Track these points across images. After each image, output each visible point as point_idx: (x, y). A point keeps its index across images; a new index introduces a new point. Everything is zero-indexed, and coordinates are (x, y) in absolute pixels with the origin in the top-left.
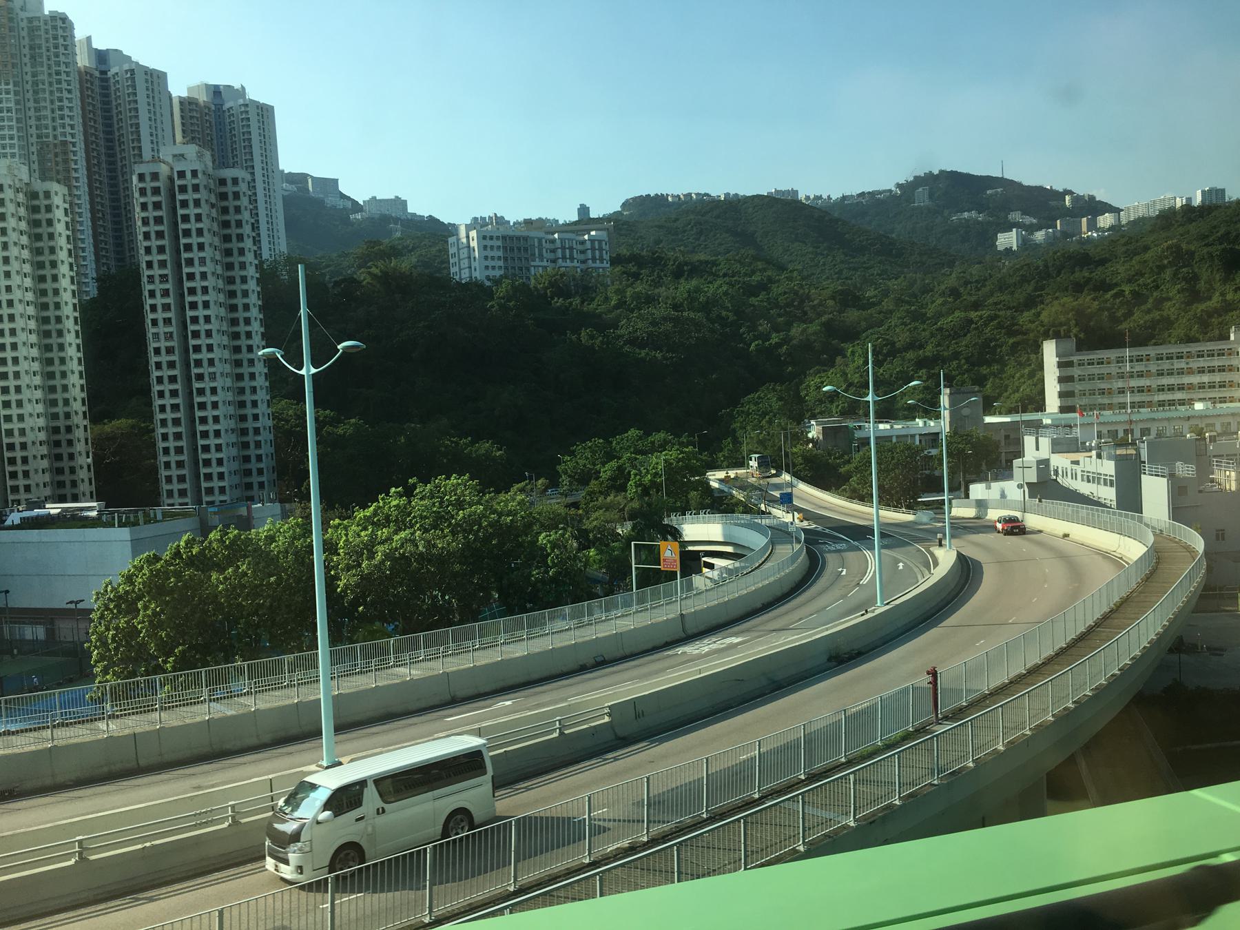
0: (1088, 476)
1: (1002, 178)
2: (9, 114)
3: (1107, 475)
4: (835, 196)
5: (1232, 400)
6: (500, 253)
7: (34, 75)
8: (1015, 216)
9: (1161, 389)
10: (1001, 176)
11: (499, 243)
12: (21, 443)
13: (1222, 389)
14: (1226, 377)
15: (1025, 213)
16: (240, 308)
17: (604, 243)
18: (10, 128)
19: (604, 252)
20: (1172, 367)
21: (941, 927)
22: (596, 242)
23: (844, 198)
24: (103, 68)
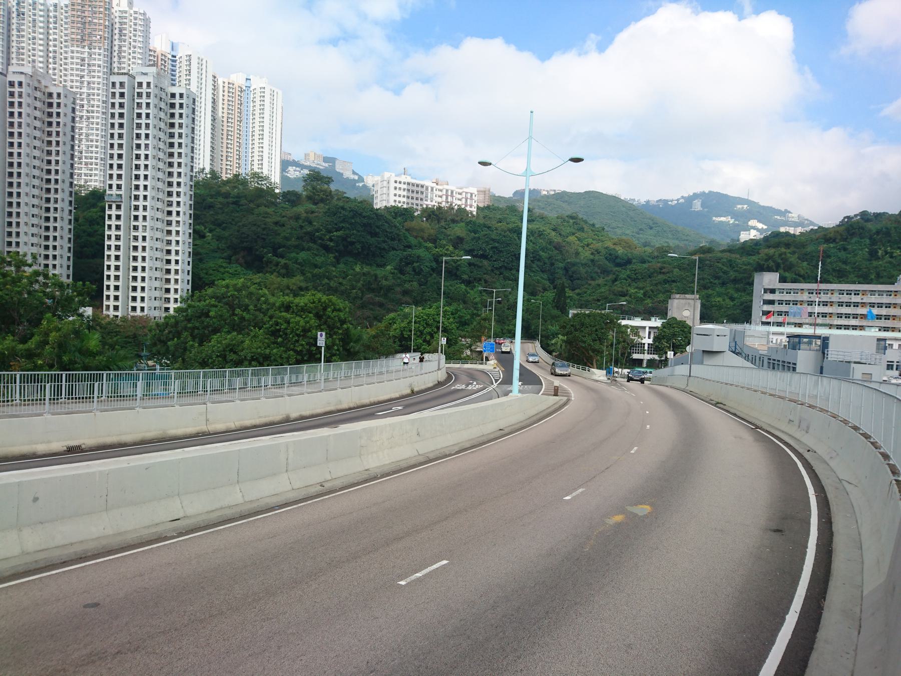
0: (774, 364)
1: (748, 199)
2: (99, 69)
3: (790, 363)
4: (643, 200)
5: (893, 329)
6: (405, 193)
7: (120, 47)
8: (753, 223)
9: (840, 316)
10: (747, 198)
11: (405, 186)
12: (114, 306)
13: (887, 321)
14: (892, 311)
15: (759, 221)
16: (175, 184)
17: (474, 195)
18: (99, 77)
19: (474, 201)
20: (850, 301)
21: (786, 645)
22: (469, 194)
23: (648, 202)
24: (174, 54)
